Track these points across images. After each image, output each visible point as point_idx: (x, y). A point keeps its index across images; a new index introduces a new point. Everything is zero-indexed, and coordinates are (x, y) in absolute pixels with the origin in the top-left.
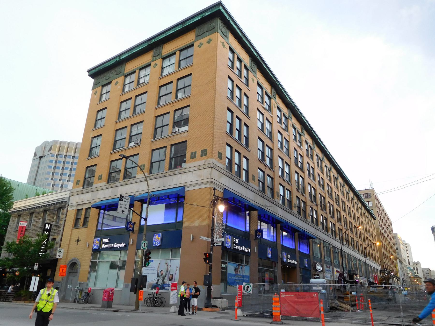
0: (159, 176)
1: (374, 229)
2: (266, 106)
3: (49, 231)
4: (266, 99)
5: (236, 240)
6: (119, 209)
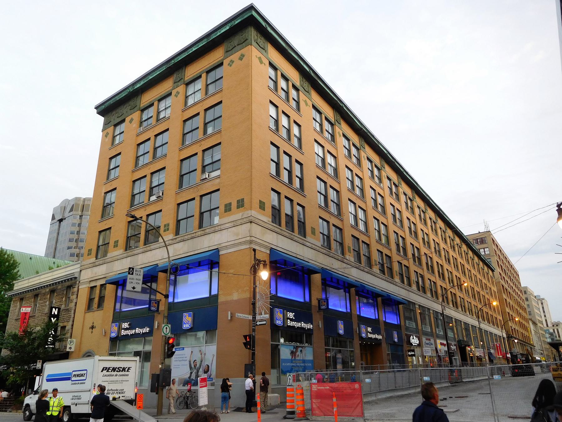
0: (186, 237)
1: (493, 282)
2: (326, 135)
3: (57, 316)
4: (326, 126)
5: (291, 315)
6: (129, 287)
